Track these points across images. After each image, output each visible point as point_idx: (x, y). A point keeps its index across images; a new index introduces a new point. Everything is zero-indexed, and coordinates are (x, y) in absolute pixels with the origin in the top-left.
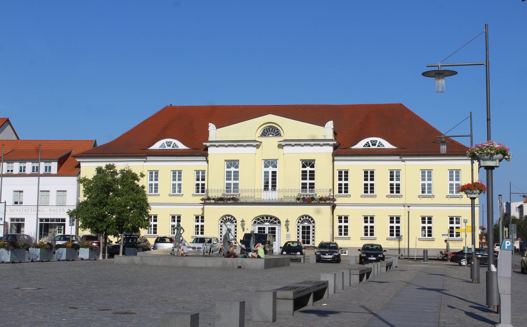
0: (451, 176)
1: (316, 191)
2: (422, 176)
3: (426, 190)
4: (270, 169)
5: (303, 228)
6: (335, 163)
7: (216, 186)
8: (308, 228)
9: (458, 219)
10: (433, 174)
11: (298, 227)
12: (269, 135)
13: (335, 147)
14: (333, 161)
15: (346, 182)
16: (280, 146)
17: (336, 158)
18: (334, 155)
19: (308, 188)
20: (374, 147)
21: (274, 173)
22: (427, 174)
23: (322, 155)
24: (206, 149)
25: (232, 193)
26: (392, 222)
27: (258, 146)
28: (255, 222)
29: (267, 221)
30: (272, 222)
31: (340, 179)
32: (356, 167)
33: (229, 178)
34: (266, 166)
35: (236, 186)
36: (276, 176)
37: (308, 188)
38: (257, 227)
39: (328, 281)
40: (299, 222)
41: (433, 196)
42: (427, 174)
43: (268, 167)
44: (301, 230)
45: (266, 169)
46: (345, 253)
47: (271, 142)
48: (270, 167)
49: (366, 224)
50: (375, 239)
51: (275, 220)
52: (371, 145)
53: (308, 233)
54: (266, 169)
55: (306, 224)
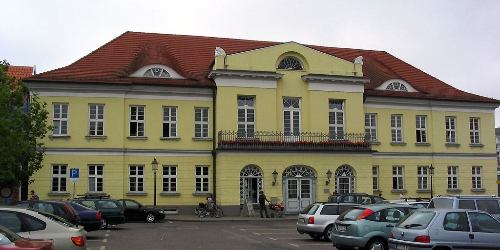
0: (367, 120)
3: (97, 131)
4: (292, 110)
5: (341, 181)
9: (64, 167)
10: (146, 112)
16: (307, 81)
17: (368, 99)
18: (366, 95)
20: (157, 77)
23: (353, 95)
24: (212, 80)
26: (198, 173)
32: (384, 112)
33: (332, 121)
34: (286, 105)
35: (251, 128)
38: (287, 180)
41: (146, 139)
42: (137, 112)
44: (339, 183)
45: (287, 109)
47: (291, 77)
48: (291, 107)
50: (178, 195)
51: (308, 172)
52: (153, 75)
54: (287, 109)
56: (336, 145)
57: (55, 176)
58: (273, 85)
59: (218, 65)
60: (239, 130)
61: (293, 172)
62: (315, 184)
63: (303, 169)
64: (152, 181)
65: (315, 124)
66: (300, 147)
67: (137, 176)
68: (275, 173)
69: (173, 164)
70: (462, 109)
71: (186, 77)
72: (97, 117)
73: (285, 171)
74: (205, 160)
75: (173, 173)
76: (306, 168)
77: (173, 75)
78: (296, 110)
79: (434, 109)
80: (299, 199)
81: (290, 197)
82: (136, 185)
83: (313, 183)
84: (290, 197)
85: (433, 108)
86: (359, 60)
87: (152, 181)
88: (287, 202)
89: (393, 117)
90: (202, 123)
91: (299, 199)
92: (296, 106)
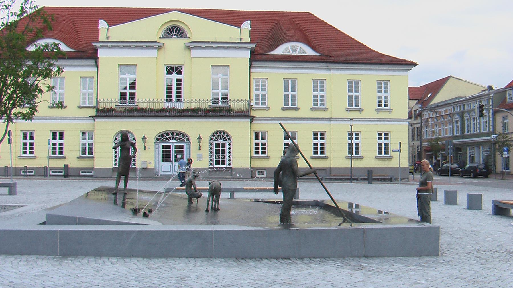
1: (137, 101)
2: (349, 87)
4: (175, 76)
5: (218, 145)
6: (252, 70)
7: (110, 97)
8: (224, 146)
11: (211, 144)
12: (172, 36)
13: (252, 52)
14: (250, 67)
15: (287, 93)
16: (189, 48)
17: (255, 64)
19: (128, 98)
21: (179, 81)
22: (353, 86)
24: (96, 51)
25: (220, 104)
27: (159, 48)
28: (158, 139)
29: (173, 138)
30: (180, 139)
31: (257, 89)
32: (274, 76)
34: (169, 73)
36: (180, 84)
37: (128, 98)
38: (161, 145)
39: (494, 201)
40: (212, 139)
42: (353, 86)
43: (171, 73)
44: (215, 149)
46: (263, 174)
47: (175, 44)
48: (174, 74)
49: (380, 142)
52: (291, 52)
53: (224, 152)
55: (221, 141)
56: (219, 110)
57: (25, 141)
58: (154, 53)
59: (102, 37)
60: (121, 98)
61: (167, 137)
62: (189, 148)
63: (178, 134)
64: (369, 147)
65: (198, 91)
66: (163, 113)
67: (354, 142)
68: (200, 138)
69: (322, 130)
70: (69, 68)
71: (320, 53)
72: (260, 90)
73: (159, 136)
74: (86, 125)
75: (386, 139)
76: (181, 134)
77: (309, 52)
78: (179, 77)
79: (333, 72)
80: (172, 163)
81: (163, 161)
82: (354, 150)
83: (187, 148)
84: (163, 161)
85: (332, 71)
86: (247, 25)
87: (369, 147)
88: (160, 166)
89: (379, 83)
90: (260, 93)
91: (172, 163)
92: (180, 73)
